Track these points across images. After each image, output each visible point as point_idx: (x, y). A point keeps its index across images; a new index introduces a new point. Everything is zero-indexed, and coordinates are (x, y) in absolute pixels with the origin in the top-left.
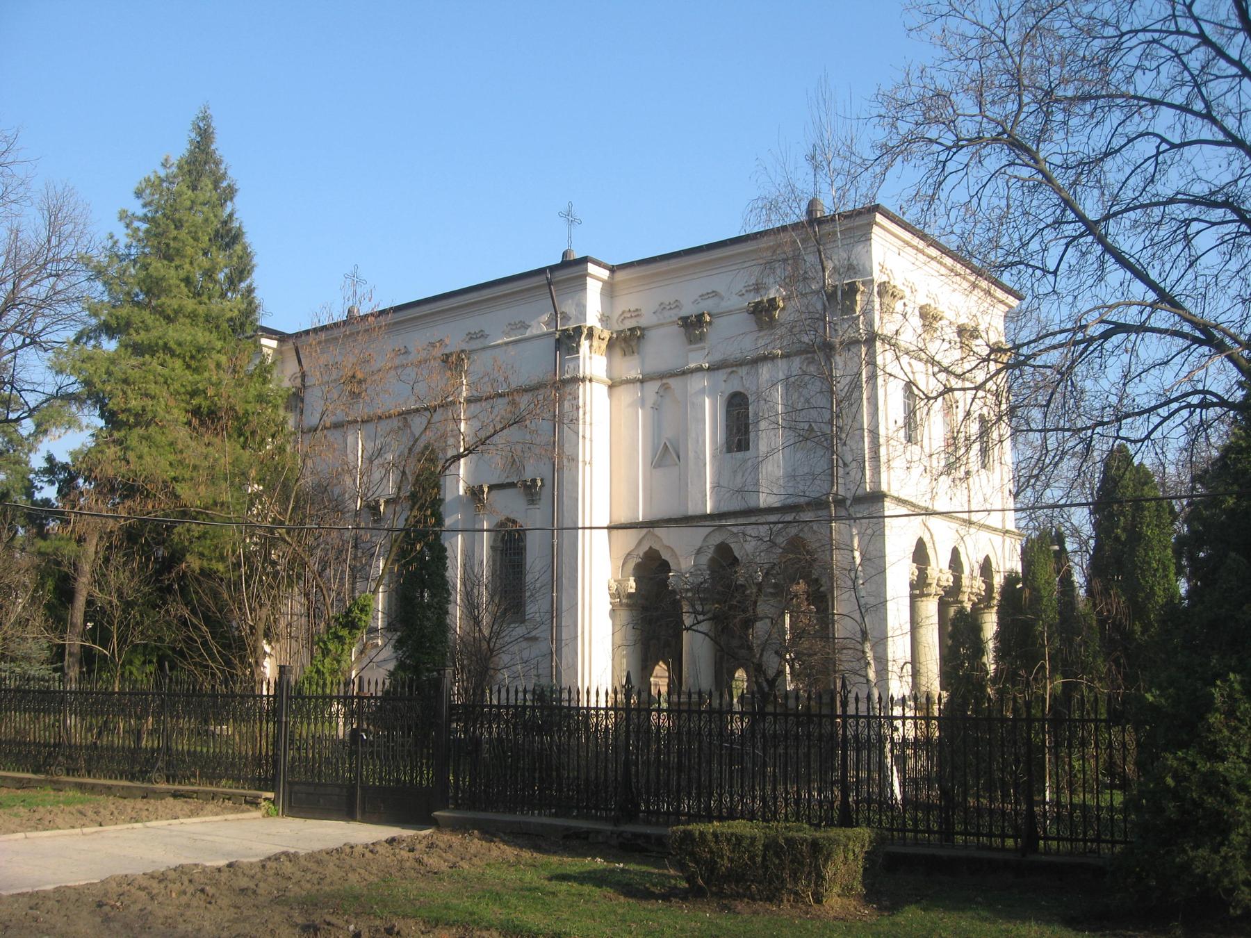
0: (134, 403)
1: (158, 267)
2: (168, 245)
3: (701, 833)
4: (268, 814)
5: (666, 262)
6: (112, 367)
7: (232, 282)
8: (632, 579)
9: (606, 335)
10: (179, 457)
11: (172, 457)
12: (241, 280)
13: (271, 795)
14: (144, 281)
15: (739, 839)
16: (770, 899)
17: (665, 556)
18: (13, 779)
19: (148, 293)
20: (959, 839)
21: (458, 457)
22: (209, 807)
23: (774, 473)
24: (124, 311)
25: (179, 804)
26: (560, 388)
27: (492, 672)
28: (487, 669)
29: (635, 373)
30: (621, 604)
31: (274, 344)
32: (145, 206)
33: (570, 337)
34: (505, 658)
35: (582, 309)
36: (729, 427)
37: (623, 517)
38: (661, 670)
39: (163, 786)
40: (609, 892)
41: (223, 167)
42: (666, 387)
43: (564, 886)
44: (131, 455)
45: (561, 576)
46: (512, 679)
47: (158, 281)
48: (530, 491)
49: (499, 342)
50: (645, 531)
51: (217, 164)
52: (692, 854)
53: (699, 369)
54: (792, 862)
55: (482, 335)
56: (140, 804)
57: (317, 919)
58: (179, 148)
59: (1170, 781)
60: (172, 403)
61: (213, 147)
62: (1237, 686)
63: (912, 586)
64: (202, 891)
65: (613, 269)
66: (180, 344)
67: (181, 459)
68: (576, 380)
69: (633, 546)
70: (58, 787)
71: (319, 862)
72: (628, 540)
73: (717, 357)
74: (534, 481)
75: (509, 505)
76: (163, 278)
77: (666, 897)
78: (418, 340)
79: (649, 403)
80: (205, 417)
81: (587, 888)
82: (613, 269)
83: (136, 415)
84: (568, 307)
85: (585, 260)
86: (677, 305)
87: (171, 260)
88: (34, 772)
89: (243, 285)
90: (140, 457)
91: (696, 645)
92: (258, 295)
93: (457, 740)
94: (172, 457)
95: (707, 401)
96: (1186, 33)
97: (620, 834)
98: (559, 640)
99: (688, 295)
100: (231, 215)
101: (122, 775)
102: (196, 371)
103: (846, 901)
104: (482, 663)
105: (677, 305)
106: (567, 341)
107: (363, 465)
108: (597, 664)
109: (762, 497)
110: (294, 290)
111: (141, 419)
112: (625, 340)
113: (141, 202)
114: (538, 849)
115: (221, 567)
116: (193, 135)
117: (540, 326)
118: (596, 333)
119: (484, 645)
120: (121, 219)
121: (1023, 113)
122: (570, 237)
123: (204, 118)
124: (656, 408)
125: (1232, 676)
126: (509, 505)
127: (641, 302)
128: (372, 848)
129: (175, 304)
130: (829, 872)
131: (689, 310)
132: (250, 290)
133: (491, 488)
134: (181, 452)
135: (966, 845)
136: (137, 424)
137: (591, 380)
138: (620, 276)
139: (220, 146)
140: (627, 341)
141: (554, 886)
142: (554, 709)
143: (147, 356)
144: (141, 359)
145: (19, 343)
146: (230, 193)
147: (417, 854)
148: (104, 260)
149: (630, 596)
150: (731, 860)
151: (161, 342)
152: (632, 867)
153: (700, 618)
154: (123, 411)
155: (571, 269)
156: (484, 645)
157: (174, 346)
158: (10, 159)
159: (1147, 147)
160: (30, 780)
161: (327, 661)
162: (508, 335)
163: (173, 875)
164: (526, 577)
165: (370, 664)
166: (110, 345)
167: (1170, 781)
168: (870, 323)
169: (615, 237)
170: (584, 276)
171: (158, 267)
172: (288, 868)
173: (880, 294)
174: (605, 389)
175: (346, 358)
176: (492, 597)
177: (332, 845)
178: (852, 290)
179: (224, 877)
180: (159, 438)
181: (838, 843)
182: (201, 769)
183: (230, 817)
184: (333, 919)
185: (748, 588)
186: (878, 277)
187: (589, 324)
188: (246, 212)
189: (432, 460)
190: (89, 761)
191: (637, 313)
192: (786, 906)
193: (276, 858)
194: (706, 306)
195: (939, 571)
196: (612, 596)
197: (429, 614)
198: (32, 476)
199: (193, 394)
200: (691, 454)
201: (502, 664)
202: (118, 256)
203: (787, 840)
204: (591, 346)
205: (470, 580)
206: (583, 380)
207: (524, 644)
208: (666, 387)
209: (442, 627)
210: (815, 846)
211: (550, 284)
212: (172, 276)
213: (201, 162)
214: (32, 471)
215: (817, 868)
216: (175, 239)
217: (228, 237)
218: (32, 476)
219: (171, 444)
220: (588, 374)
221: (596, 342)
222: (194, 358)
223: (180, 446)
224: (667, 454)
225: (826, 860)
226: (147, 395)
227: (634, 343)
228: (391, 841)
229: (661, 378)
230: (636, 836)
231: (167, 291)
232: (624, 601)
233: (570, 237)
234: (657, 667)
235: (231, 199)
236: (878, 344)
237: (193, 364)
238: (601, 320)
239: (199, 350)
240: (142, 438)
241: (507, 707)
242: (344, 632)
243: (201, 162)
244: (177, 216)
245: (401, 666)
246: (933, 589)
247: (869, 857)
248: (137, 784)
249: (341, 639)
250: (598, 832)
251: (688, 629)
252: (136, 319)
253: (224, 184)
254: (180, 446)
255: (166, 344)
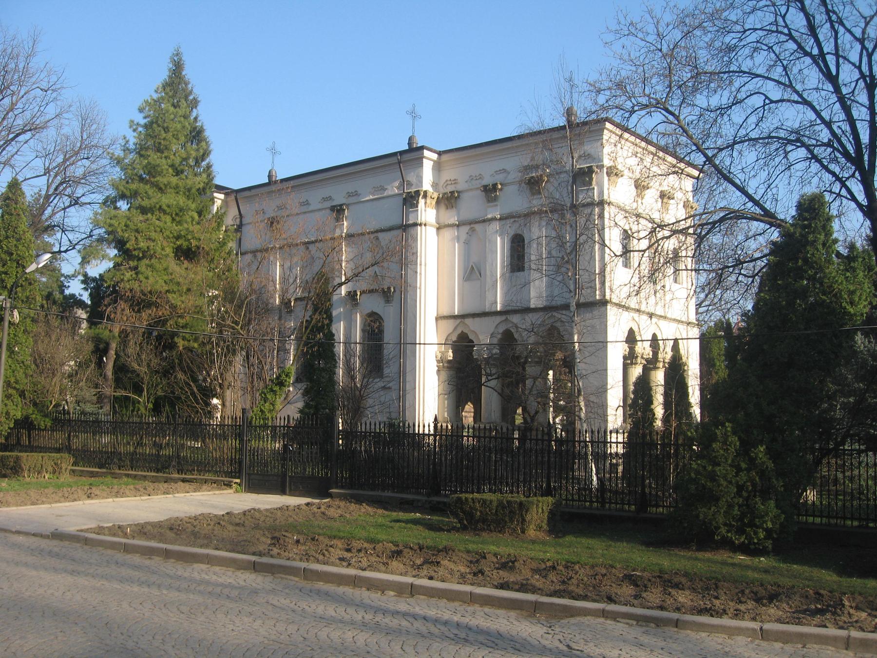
0: (143, 245)
1: (154, 157)
2: (160, 143)
3: (466, 498)
4: (237, 491)
5: (473, 150)
6: (128, 222)
7: (197, 162)
8: (450, 351)
9: (435, 195)
10: (170, 277)
11: (166, 278)
12: (203, 160)
13: (238, 481)
14: (146, 166)
15: (485, 501)
16: (500, 532)
17: (471, 337)
18: (88, 471)
19: (149, 173)
20: (607, 506)
21: (341, 284)
22: (205, 487)
23: (537, 292)
24: (134, 186)
25: (187, 485)
26: (407, 228)
27: (362, 409)
28: (359, 407)
29: (454, 220)
30: (443, 367)
31: (222, 196)
32: (145, 118)
33: (412, 197)
34: (370, 401)
35: (420, 181)
36: (512, 256)
37: (445, 312)
38: (469, 407)
39: (177, 476)
40: (421, 528)
41: (190, 86)
42: (473, 230)
43: (398, 524)
44: (141, 277)
45: (407, 344)
46: (374, 418)
47: (154, 167)
48: (387, 295)
49: (368, 198)
50: (458, 321)
51: (186, 84)
52: (462, 509)
53: (494, 219)
54: (510, 512)
55: (356, 194)
56: (166, 485)
57: (277, 534)
58: (163, 74)
59: (693, 475)
60: (165, 244)
61: (183, 73)
62: (729, 429)
63: (625, 358)
64: (219, 523)
65: (440, 153)
66: (169, 206)
67: (163, 274)
68: (415, 225)
69: (451, 330)
70: (115, 476)
71: (272, 513)
72: (449, 326)
73: (507, 210)
74: (389, 288)
75: (373, 304)
76: (158, 166)
77: (448, 531)
78: (315, 196)
79: (462, 240)
80: (186, 254)
81: (409, 526)
82: (440, 153)
83: (144, 252)
84: (411, 177)
85: (422, 148)
86: (481, 177)
87: (162, 152)
88: (99, 468)
89: (204, 164)
90: (147, 278)
91: (490, 396)
92: (215, 168)
93: (344, 452)
94: (166, 278)
95: (499, 239)
96: (781, 33)
97: (430, 502)
98: (404, 391)
99: (488, 170)
100: (196, 119)
101: (150, 469)
102: (179, 223)
103: (538, 533)
104: (356, 404)
105: (481, 177)
106: (411, 200)
107: (280, 276)
108: (428, 404)
109: (532, 302)
110: (236, 163)
111: (146, 254)
112: (447, 199)
113: (142, 115)
114: (386, 509)
115: (196, 345)
116: (171, 66)
117: (393, 189)
118: (429, 195)
119: (357, 393)
120: (131, 127)
121: (675, 93)
122: (413, 127)
123: (177, 55)
124: (467, 243)
125: (727, 424)
126: (373, 304)
127: (457, 175)
128: (299, 507)
129: (165, 180)
130: (528, 517)
131: (488, 181)
132: (209, 167)
133: (362, 293)
134: (171, 274)
135: (610, 509)
136: (144, 257)
137: (425, 225)
138: (445, 157)
139: (188, 72)
140: (448, 200)
141: (393, 524)
142: (400, 434)
143: (149, 215)
144: (146, 217)
145: (67, 204)
146: (195, 103)
147: (323, 509)
148: (122, 154)
149: (449, 362)
150: (481, 512)
151: (158, 206)
152: (435, 518)
153: (490, 378)
154: (135, 250)
155: (413, 153)
156: (357, 393)
157: (166, 208)
158: (59, 86)
159: (758, 101)
160: (98, 472)
161: (267, 404)
162: (373, 194)
163: (200, 518)
164: (385, 351)
165: (289, 406)
166: (123, 205)
167: (693, 475)
168: (601, 193)
169: (443, 131)
170: (421, 158)
171: (154, 157)
172: (257, 515)
173: (608, 174)
174: (435, 230)
175: (270, 206)
176: (362, 364)
177: (275, 506)
178: (590, 171)
179: (226, 518)
180: (158, 266)
181: (532, 503)
182: (198, 467)
183: (217, 492)
184: (286, 534)
185: (520, 357)
186: (607, 162)
187: (424, 189)
188: (207, 116)
189: (327, 281)
190: (132, 460)
191: (455, 182)
192: (507, 535)
193: (249, 511)
194: (499, 178)
195: (644, 349)
196: (438, 361)
197: (324, 374)
198: (63, 279)
199: (178, 238)
200: (488, 273)
201: (368, 405)
202: (128, 149)
203: (508, 502)
204: (426, 203)
205: (349, 354)
206: (421, 225)
207: (382, 393)
208: (473, 230)
209: (332, 382)
210: (521, 504)
211: (399, 163)
212: (164, 164)
213: (176, 86)
214: (63, 275)
215: (522, 515)
216: (164, 139)
217: (197, 135)
218: (63, 279)
219: (165, 269)
220: (423, 221)
221: (429, 200)
222: (178, 215)
223: (170, 271)
224: (473, 272)
225: (526, 512)
226: (150, 239)
227: (453, 201)
228: (308, 504)
229: (470, 224)
230: (439, 503)
231: (160, 174)
232: (446, 365)
233: (413, 127)
234: (467, 406)
235: (196, 107)
236: (606, 206)
237: (178, 219)
238: (432, 186)
239: (181, 210)
240: (147, 266)
241: (370, 433)
242: (276, 388)
243: (176, 86)
244: (165, 125)
245: (307, 405)
246: (639, 360)
247: (551, 512)
248: (161, 474)
249: (274, 392)
250: (419, 501)
251: (769, 217)
252: (141, 191)
253: (191, 98)
254: (170, 271)
255: (160, 207)
